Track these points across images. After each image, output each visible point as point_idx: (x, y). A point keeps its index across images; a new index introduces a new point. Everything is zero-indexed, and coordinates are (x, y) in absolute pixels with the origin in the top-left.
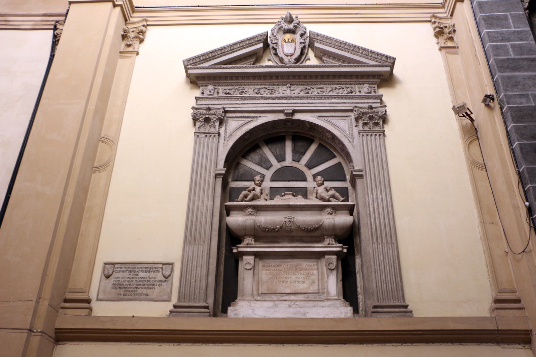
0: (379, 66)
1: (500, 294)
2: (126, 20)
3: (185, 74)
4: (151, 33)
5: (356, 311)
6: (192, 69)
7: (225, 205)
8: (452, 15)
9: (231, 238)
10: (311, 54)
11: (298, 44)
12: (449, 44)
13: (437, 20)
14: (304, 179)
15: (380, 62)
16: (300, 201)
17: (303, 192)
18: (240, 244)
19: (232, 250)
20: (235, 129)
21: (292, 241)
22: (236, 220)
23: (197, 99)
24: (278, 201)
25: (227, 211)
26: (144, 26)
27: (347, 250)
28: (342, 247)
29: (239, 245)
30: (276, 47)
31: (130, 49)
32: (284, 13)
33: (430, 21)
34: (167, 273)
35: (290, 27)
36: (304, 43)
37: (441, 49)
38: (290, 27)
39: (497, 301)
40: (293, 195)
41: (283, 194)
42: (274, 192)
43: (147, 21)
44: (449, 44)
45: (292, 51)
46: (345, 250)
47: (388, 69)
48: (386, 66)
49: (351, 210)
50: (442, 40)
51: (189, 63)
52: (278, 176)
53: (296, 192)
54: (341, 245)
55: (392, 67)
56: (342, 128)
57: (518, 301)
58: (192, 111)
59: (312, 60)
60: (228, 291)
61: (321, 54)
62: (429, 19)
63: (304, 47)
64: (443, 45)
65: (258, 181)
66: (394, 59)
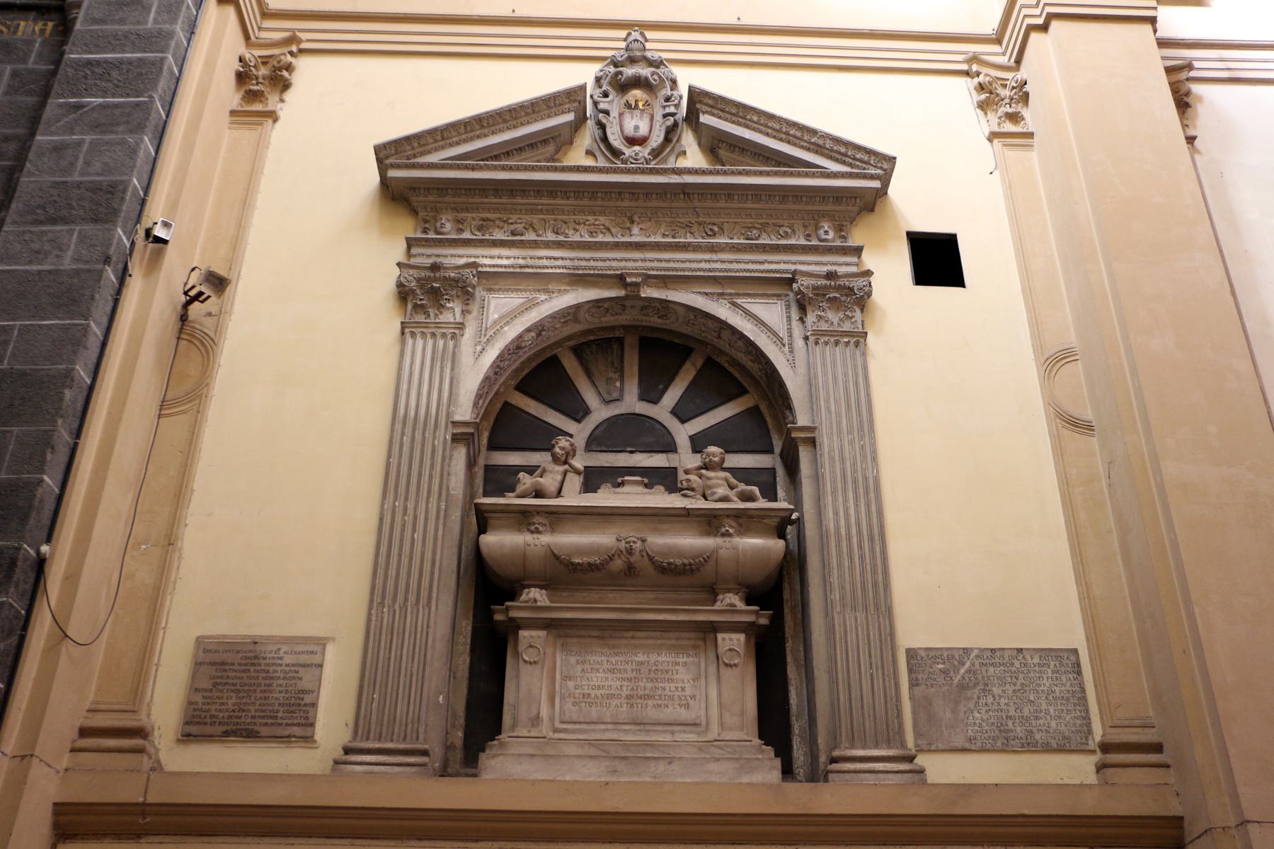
0: (858, 176)
1: (1113, 730)
2: (247, 37)
3: (375, 178)
4: (307, 72)
5: (788, 771)
6: (398, 167)
7: (476, 505)
8: (1018, 62)
9: (489, 591)
10: (688, 140)
11: (658, 117)
12: (1009, 127)
13: (984, 70)
14: (669, 447)
15: (850, 165)
16: (660, 499)
17: (667, 479)
18: (512, 600)
19: (490, 614)
20: (505, 320)
21: (635, 594)
22: (500, 541)
23: (410, 243)
24: (605, 498)
25: (484, 520)
26: (291, 53)
27: (771, 622)
28: (756, 613)
29: (508, 603)
30: (604, 121)
31: (258, 107)
32: (614, 43)
33: (967, 73)
34: (989, 653)
35: (632, 77)
36: (673, 115)
37: (993, 136)
38: (632, 77)
39: (84, 732)
40: (646, 486)
41: (620, 480)
42: (593, 479)
43: (299, 41)
44: (1009, 127)
45: (644, 130)
46: (763, 621)
47: (876, 184)
48: (872, 177)
49: (782, 525)
50: (992, 122)
51: (387, 154)
52: (596, 442)
53: (654, 478)
54: (755, 608)
55: (886, 180)
56: (764, 322)
57: (1157, 748)
58: (397, 271)
59: (693, 156)
60: (483, 717)
61: (716, 145)
62: (965, 67)
63: (675, 125)
64: (996, 129)
65: (563, 449)
66: (892, 160)
